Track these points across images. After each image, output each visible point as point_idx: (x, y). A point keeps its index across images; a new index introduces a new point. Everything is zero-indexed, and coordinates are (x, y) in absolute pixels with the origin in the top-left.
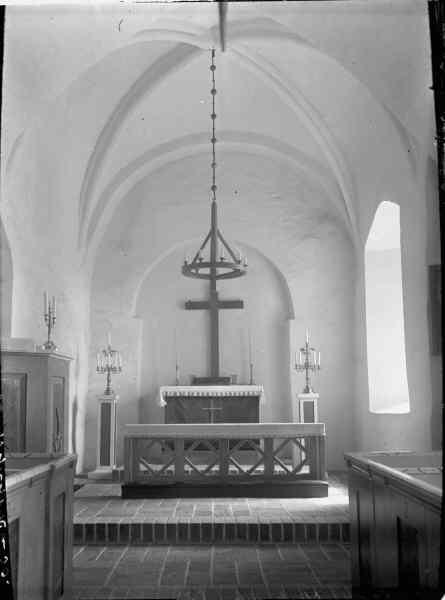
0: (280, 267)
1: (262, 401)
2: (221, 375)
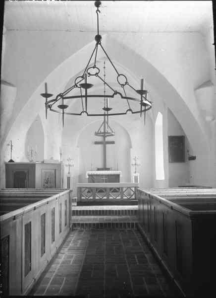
0: (127, 129)
1: (121, 176)
2: (107, 167)
